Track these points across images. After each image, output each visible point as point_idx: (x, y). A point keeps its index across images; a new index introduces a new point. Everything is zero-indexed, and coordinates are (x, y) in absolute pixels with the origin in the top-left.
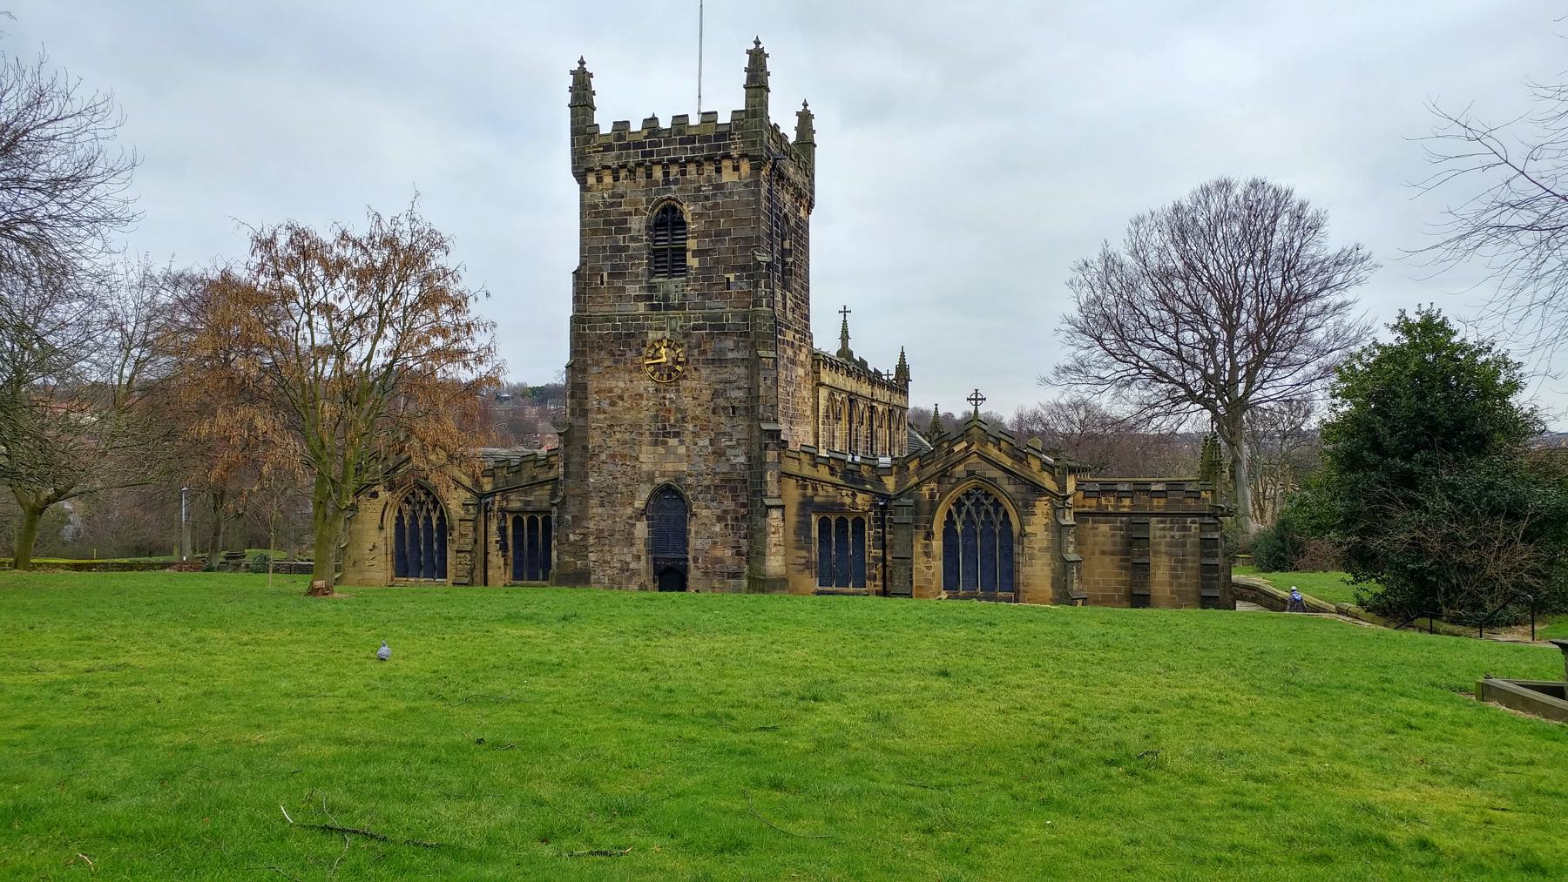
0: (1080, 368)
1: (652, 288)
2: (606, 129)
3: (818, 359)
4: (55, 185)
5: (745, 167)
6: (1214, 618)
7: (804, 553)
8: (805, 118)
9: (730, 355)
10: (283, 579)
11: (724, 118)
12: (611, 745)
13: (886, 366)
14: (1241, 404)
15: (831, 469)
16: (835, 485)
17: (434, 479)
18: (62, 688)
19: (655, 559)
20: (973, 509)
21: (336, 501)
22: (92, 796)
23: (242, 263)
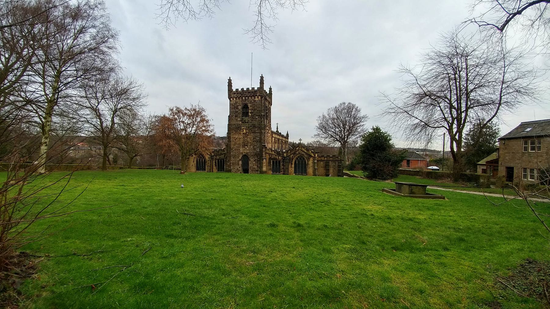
0: (318, 135)
2: (234, 90)
3: (272, 132)
4: (134, 99)
5: (260, 97)
6: (340, 178)
8: (270, 89)
10: (176, 171)
11: (256, 89)
12: (235, 200)
13: (285, 134)
14: (346, 142)
17: (203, 153)
18: (138, 189)
21: (185, 157)
22: (144, 207)
23: (167, 114)
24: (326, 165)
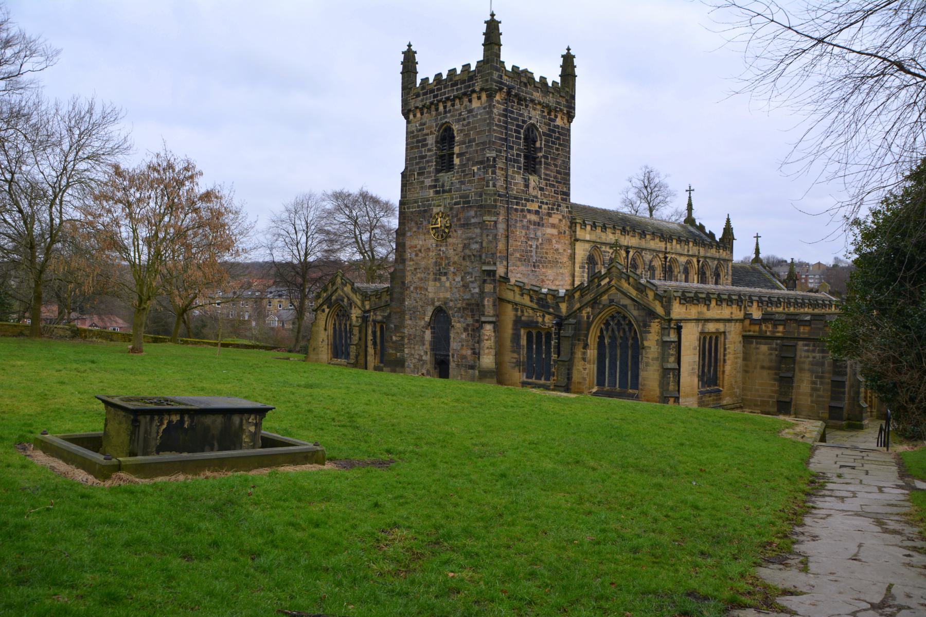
1: (437, 180)
7: (516, 355)
9: (473, 221)
15: (531, 297)
16: (533, 309)
19: (436, 355)
20: (615, 327)
24: (782, 359)
